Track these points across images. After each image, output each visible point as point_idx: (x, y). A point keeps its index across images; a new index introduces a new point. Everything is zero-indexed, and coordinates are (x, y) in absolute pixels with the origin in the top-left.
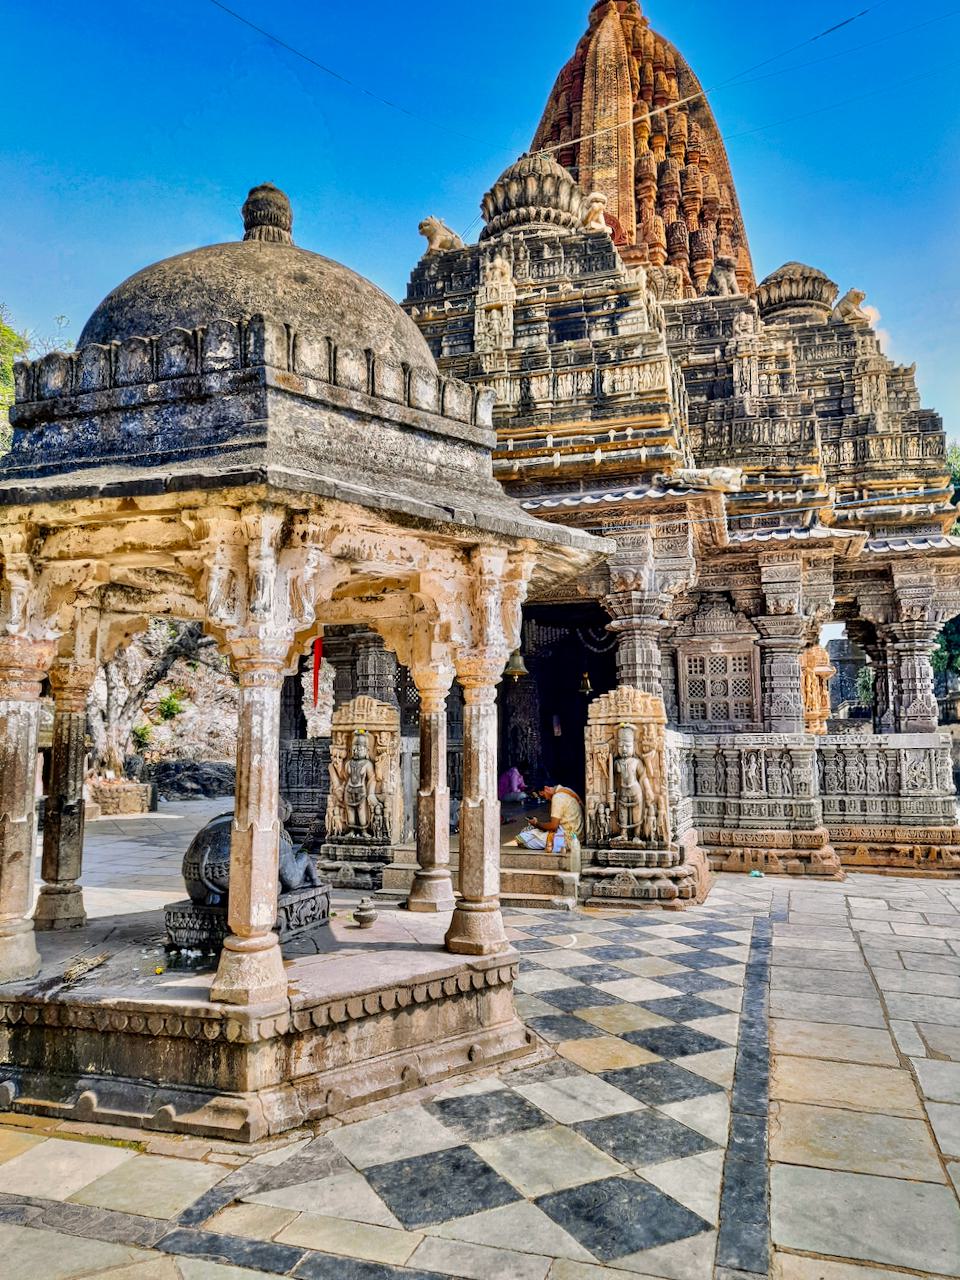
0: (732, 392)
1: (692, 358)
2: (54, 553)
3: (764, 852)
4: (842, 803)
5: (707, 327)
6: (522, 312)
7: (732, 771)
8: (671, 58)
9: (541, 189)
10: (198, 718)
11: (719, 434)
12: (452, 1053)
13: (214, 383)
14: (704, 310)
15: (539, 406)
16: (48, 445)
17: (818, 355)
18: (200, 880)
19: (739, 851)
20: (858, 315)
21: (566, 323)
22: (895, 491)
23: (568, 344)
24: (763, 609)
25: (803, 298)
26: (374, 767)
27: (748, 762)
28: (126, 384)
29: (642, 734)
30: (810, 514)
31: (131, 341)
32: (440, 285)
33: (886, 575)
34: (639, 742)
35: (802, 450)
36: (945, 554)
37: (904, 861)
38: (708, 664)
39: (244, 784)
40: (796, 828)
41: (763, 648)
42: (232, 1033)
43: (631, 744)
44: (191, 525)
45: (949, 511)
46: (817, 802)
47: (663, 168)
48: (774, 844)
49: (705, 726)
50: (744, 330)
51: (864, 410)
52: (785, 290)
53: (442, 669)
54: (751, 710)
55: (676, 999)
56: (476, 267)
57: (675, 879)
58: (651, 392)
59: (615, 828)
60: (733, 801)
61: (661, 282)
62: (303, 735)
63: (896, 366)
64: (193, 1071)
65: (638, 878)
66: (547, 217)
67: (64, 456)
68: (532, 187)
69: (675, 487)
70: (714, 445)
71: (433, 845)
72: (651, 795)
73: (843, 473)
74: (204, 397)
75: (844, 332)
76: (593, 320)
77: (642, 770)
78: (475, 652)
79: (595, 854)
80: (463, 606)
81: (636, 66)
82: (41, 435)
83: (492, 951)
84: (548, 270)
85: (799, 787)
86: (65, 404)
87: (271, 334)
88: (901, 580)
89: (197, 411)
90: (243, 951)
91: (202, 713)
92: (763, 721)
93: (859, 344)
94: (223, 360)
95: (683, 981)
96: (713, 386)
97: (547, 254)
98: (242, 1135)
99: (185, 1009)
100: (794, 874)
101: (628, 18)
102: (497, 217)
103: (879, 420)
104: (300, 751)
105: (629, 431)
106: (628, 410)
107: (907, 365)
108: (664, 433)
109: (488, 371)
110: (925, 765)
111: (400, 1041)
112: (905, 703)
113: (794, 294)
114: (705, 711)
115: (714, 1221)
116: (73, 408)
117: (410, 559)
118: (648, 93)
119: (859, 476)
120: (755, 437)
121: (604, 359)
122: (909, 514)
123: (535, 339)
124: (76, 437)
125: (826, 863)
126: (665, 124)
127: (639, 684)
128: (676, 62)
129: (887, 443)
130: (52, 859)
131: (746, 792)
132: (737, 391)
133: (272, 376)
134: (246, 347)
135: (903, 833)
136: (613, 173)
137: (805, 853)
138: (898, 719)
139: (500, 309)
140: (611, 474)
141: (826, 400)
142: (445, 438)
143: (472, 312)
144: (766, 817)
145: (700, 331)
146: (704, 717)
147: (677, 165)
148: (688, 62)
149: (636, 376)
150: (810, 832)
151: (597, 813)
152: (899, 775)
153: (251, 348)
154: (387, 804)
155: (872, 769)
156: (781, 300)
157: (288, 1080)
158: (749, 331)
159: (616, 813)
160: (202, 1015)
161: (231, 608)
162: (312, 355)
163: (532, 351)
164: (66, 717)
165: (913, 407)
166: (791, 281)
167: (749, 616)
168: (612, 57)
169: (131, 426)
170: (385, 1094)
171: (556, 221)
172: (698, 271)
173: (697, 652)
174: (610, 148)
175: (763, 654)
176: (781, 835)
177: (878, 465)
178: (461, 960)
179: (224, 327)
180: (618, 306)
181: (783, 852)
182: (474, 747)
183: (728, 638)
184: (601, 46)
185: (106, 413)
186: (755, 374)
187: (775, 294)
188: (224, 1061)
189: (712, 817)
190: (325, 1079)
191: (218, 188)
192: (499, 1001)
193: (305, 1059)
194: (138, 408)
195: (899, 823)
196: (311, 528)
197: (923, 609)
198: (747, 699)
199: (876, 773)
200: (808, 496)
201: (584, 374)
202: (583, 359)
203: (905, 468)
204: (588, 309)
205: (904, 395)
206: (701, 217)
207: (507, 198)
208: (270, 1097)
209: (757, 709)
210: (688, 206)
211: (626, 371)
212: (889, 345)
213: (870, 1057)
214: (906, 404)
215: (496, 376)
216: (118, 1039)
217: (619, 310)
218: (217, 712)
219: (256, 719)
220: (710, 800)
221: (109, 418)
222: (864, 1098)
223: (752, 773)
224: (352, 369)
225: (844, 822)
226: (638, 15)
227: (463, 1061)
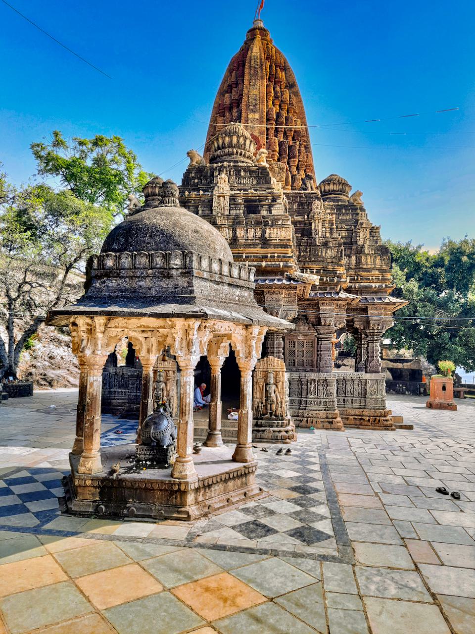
0: (311, 235)
1: (296, 218)
2: (113, 326)
3: (315, 420)
4: (344, 400)
5: (301, 204)
6: (233, 199)
7: (304, 387)
8: (282, 61)
9: (238, 141)
10: (43, 349)
11: (304, 251)
12: (240, 494)
13: (174, 272)
14: (300, 197)
15: (240, 241)
16: (108, 287)
17: (344, 217)
18: (150, 437)
19: (306, 419)
20: (360, 202)
21: (252, 206)
22: (371, 278)
23: (252, 215)
24: (319, 323)
25: (338, 191)
26: (166, 386)
27: (311, 384)
28: (138, 268)
29: (277, 375)
30: (339, 287)
31: (141, 253)
32: (196, 181)
33: (365, 310)
34: (275, 378)
35: (337, 260)
36: (387, 304)
37: (366, 423)
38: (296, 344)
39: (184, 408)
40: (328, 410)
41: (318, 338)
42: (183, 488)
43: (272, 379)
44: (170, 323)
45: (390, 287)
46: (336, 400)
47: (278, 115)
48: (319, 417)
49: (294, 369)
50: (317, 208)
51: (360, 243)
52: (331, 187)
53: (221, 358)
54: (312, 363)
55: (300, 477)
56: (212, 175)
57: (287, 432)
58: (284, 240)
59: (265, 412)
60: (304, 399)
61: (277, 169)
62: (116, 366)
63: (373, 225)
64: (168, 500)
65: (274, 431)
66: (241, 154)
67: (115, 292)
68: (235, 139)
69: (294, 280)
70: (303, 256)
71: (216, 423)
72: (279, 399)
73: (351, 269)
74: (169, 277)
75: (354, 208)
76: (262, 206)
77: (276, 389)
78: (247, 360)
79: (257, 422)
80: (243, 344)
81: (268, 64)
82: (104, 282)
83: (250, 461)
84: (243, 181)
85: (329, 394)
86: (115, 272)
87: (194, 258)
88: (371, 313)
89: (167, 281)
90: (184, 462)
91: (44, 347)
92: (317, 367)
93: (360, 215)
94: (177, 265)
95: (300, 470)
96: (304, 231)
97: (242, 174)
98: (188, 518)
99: (166, 480)
100: (327, 429)
101: (264, 40)
102: (219, 151)
103: (366, 248)
104: (116, 373)
105: (276, 255)
106: (276, 246)
107: (378, 226)
108: (289, 257)
109: (219, 224)
110: (375, 386)
111: (226, 491)
112: (369, 361)
113: (335, 189)
114: (294, 363)
115: (331, 533)
116: (118, 274)
117: (231, 330)
118: (273, 79)
119: (357, 270)
120: (319, 254)
121: (266, 224)
122: (376, 287)
123: (238, 212)
124: (119, 285)
125: (339, 424)
126: (279, 94)
127: (275, 355)
128: (284, 63)
129: (369, 258)
130: (81, 429)
131: (309, 396)
132: (313, 234)
133: (195, 272)
134: (186, 262)
135: (367, 412)
136: (257, 116)
137: (331, 420)
138: (366, 368)
139: (224, 197)
140: (268, 271)
141: (346, 237)
142: (240, 287)
143: (212, 196)
144: (316, 406)
145: (299, 206)
146: (294, 365)
147: (284, 113)
148: (290, 64)
149: (279, 232)
150: (332, 412)
151: (258, 406)
152: (366, 389)
153: (188, 262)
154: (172, 401)
155: (356, 387)
156: (329, 190)
157: (197, 503)
158: (319, 207)
159: (266, 406)
160: (172, 482)
161: (181, 350)
162: (205, 263)
163: (237, 216)
164: (86, 375)
165: (379, 244)
166: (334, 183)
167: (313, 325)
168: (258, 61)
169: (141, 283)
170: (224, 507)
171: (244, 156)
172: (292, 164)
173: (293, 339)
174: (256, 104)
175: (318, 341)
176: (323, 414)
177: (365, 267)
178: (242, 465)
179: (178, 254)
180: (272, 201)
181: (323, 420)
182: (245, 392)
183: (305, 334)
184: (253, 54)
185: (131, 278)
186: (320, 227)
187: (327, 188)
188: (179, 497)
189: (296, 405)
190: (208, 502)
191: (103, 128)
192: (251, 478)
193: (201, 496)
194: (145, 277)
195: (365, 408)
196: (208, 325)
197: (378, 325)
198: (311, 358)
199: (357, 388)
200: (339, 279)
201: (258, 230)
202: (258, 223)
203: (374, 269)
204: (260, 201)
205: (375, 238)
206: (293, 139)
207: (223, 143)
208: (194, 508)
209: (315, 363)
210: (288, 133)
211: (275, 229)
212: (372, 215)
213: (366, 493)
214: (376, 243)
215: (223, 226)
216: (140, 491)
217: (273, 203)
218: (52, 346)
219: (188, 387)
220: (295, 398)
221: (132, 279)
222: (366, 505)
223: (312, 389)
224: (216, 267)
225: (344, 407)
226: (268, 38)
227: (243, 497)
